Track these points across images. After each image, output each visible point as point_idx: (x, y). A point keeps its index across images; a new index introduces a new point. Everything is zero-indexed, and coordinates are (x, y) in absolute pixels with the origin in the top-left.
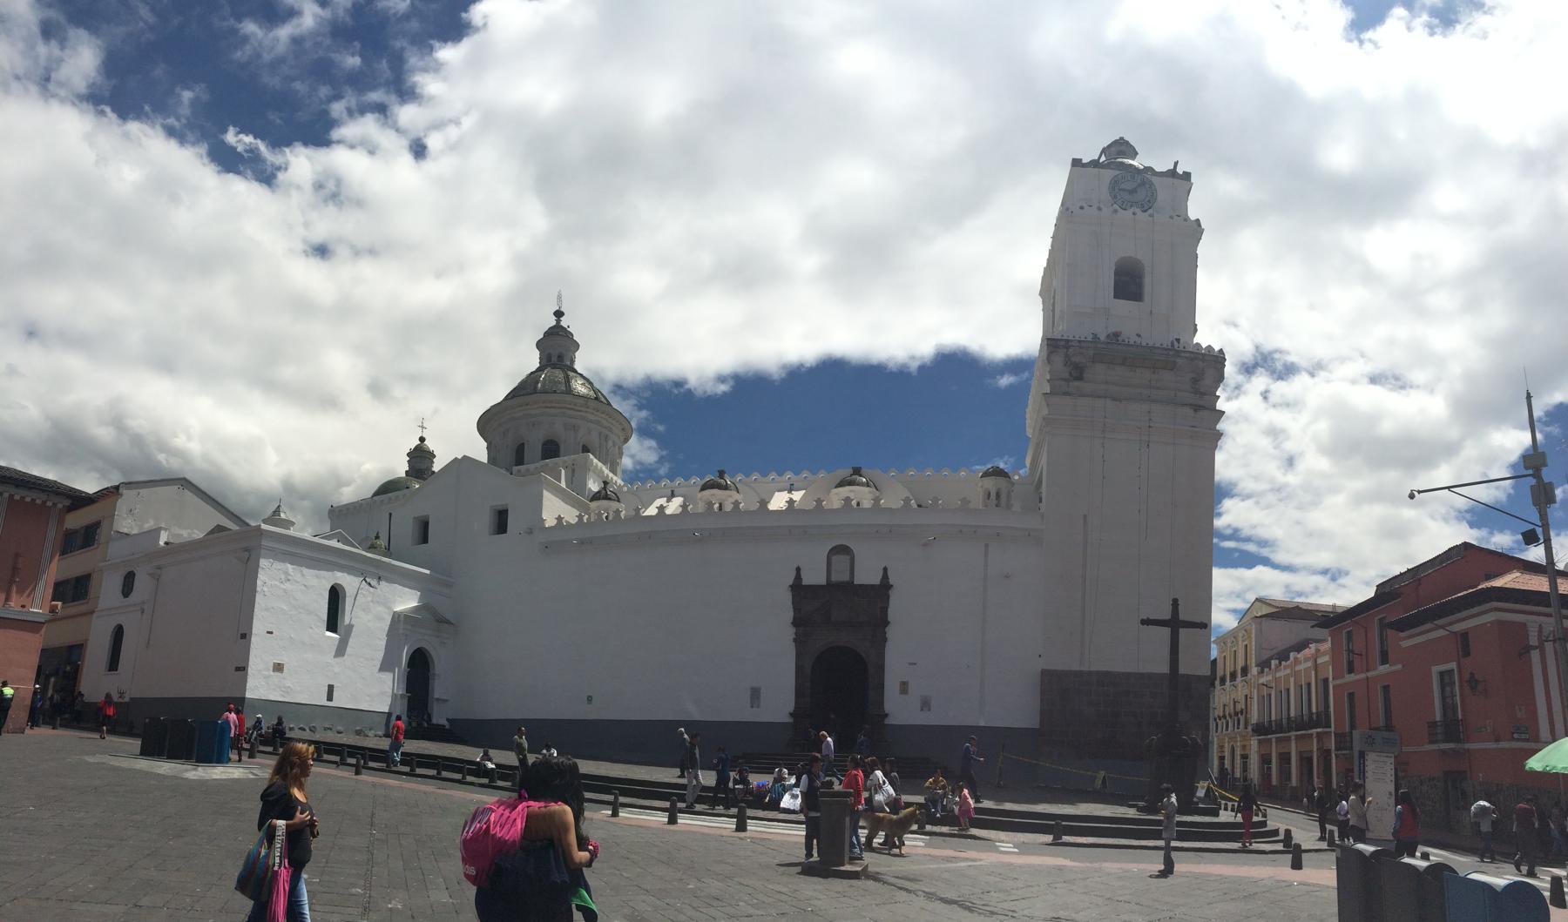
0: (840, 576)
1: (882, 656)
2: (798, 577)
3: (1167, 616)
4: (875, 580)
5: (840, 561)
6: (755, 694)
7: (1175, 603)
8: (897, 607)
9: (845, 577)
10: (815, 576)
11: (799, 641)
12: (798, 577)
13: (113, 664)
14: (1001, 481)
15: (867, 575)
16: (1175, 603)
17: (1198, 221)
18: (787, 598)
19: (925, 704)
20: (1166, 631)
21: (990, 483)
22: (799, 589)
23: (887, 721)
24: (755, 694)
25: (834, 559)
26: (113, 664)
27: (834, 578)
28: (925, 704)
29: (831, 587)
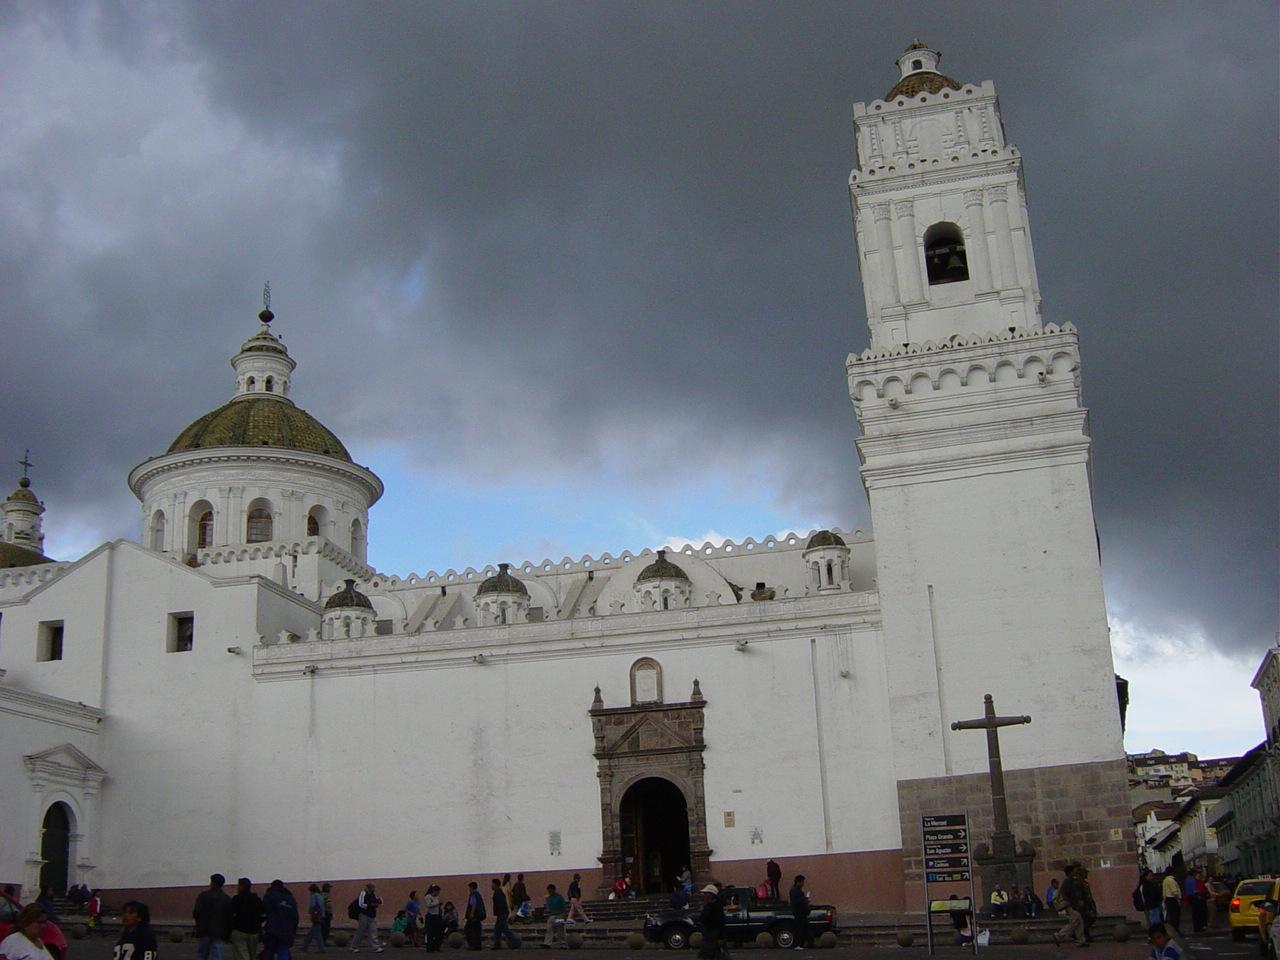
0: (647, 695)
1: (699, 783)
2: (598, 700)
3: (981, 715)
4: (686, 697)
5: (646, 678)
6: (555, 840)
7: (989, 700)
8: (713, 728)
9: (653, 697)
10: (618, 697)
11: (606, 775)
12: (598, 700)
13: (294, 577)
14: (832, 554)
15: (678, 693)
16: (989, 700)
17: (240, 880)
18: (588, 724)
19: (756, 837)
20: (981, 715)
21: (820, 556)
22: (600, 714)
23: (712, 859)
24: (555, 840)
25: (639, 674)
26: (294, 577)
27: (641, 698)
28: (756, 837)
29: (641, 709)
